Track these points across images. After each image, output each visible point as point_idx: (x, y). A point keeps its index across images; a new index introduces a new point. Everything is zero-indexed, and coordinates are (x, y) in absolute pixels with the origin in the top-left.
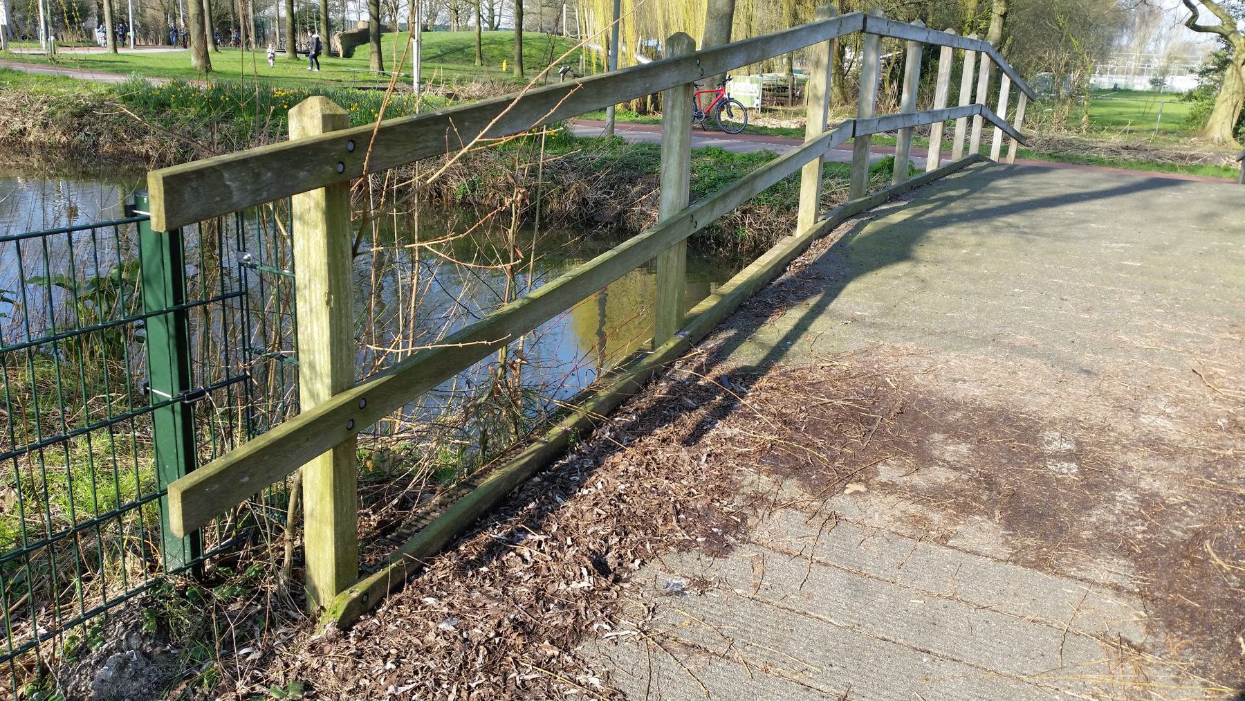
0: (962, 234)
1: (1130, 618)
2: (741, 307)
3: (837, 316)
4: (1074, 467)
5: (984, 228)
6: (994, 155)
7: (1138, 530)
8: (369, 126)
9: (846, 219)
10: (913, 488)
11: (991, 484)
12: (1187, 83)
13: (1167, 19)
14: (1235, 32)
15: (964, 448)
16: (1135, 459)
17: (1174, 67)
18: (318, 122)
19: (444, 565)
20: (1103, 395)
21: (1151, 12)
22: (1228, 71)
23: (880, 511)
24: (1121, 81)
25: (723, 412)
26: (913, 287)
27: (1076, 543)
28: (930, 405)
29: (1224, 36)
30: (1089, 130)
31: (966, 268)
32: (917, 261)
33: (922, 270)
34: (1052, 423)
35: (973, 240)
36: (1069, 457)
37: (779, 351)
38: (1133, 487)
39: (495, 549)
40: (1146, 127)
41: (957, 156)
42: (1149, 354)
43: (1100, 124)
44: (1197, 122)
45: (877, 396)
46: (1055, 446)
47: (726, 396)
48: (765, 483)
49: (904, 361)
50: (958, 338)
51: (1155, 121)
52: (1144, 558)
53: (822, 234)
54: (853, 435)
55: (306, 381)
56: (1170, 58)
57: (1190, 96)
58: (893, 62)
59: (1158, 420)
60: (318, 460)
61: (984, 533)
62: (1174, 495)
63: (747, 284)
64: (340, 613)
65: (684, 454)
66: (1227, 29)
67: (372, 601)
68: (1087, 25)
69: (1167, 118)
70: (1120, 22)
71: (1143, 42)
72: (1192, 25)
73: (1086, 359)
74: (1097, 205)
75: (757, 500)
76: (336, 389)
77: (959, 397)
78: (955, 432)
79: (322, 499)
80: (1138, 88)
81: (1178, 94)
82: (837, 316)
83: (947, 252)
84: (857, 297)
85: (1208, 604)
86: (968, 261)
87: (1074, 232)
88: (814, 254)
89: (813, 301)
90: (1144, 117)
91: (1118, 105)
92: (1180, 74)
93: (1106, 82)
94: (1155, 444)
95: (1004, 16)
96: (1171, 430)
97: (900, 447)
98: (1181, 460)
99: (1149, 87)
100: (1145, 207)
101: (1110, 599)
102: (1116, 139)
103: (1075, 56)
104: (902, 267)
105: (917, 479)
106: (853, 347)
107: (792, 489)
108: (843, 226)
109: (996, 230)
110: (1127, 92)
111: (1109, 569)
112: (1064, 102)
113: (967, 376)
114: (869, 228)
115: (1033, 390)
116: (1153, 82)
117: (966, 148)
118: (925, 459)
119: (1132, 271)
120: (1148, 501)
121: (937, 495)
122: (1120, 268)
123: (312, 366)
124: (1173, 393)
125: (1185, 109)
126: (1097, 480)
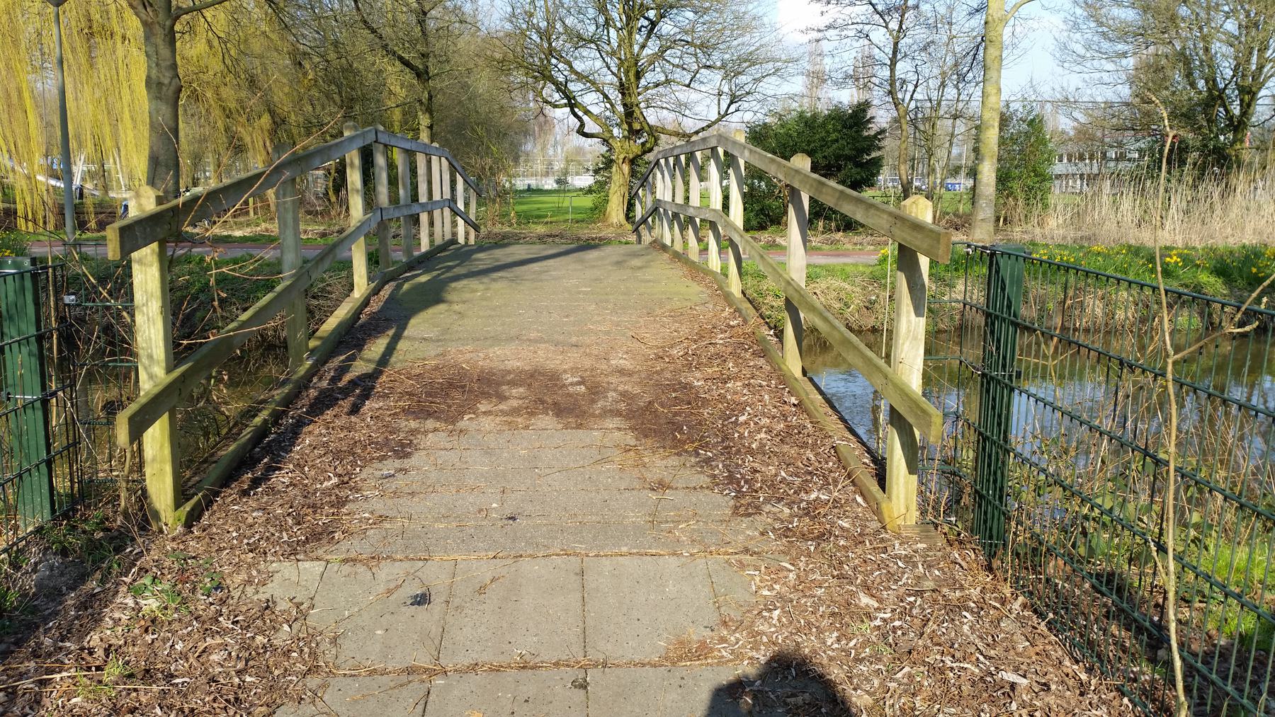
0: (473, 283)
1: (630, 439)
2: (340, 342)
3: (409, 338)
4: (583, 388)
5: (486, 280)
6: (461, 240)
7: (623, 406)
8: (174, 202)
9: (387, 282)
10: (501, 411)
11: (543, 402)
12: (586, 180)
13: (558, 130)
14: (612, 137)
15: (521, 390)
16: (613, 379)
17: (572, 168)
18: (153, 200)
19: (232, 492)
20: (589, 355)
21: (546, 122)
22: (614, 169)
23: (487, 423)
24: (533, 182)
25: (366, 396)
26: (455, 317)
27: (593, 415)
28: (494, 374)
29: (605, 141)
30: (519, 224)
31: (484, 303)
32: (451, 303)
33: (456, 307)
34: (565, 371)
35: (481, 287)
36: (579, 383)
37: (384, 361)
38: (615, 390)
39: (265, 478)
40: (561, 218)
41: (439, 241)
42: (608, 333)
43: (526, 218)
44: (598, 211)
45: (462, 374)
46: (570, 380)
47: (365, 386)
48: (413, 424)
49: (468, 356)
50: (496, 340)
51: (567, 213)
52: (629, 415)
53: (376, 292)
54: (456, 394)
55: (145, 368)
56: (568, 161)
57: (590, 191)
58: (333, 171)
59: (620, 360)
60: (157, 424)
61: (547, 421)
62: (637, 390)
63: (340, 325)
64: (183, 519)
65: (353, 418)
66: (607, 135)
67: (196, 514)
68: (502, 135)
69: (576, 210)
70: (525, 131)
71: (544, 148)
72: (581, 132)
73: (574, 339)
74: (551, 262)
75: (413, 432)
76: (169, 370)
77: (509, 368)
78: (513, 383)
79: (162, 446)
80: (546, 187)
81: (581, 189)
82: (409, 338)
83: (467, 296)
84: (418, 325)
85: (661, 425)
86: (483, 298)
87: (544, 277)
88: (375, 306)
89: (391, 332)
90: (559, 210)
91: (535, 202)
92: (577, 174)
93: (521, 184)
94: (622, 372)
95: (431, 127)
96: (627, 364)
97: (487, 396)
98: (636, 376)
99: (555, 186)
100: (582, 261)
101: (616, 433)
102: (541, 229)
103: (496, 161)
104: (442, 307)
105: (501, 407)
106: (433, 353)
107: (430, 424)
108: (387, 287)
109: (494, 280)
110: (540, 191)
111: (611, 423)
112: (494, 201)
113: (509, 357)
114: (406, 286)
115: (547, 358)
116: (558, 182)
117: (432, 242)
118: (502, 398)
119: (586, 293)
120: (624, 394)
121: (515, 411)
122: (579, 293)
123: (150, 357)
124: (625, 348)
125: (588, 201)
126: (595, 391)
